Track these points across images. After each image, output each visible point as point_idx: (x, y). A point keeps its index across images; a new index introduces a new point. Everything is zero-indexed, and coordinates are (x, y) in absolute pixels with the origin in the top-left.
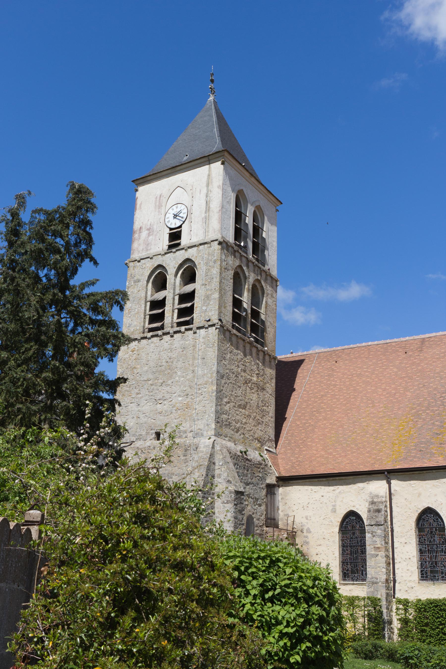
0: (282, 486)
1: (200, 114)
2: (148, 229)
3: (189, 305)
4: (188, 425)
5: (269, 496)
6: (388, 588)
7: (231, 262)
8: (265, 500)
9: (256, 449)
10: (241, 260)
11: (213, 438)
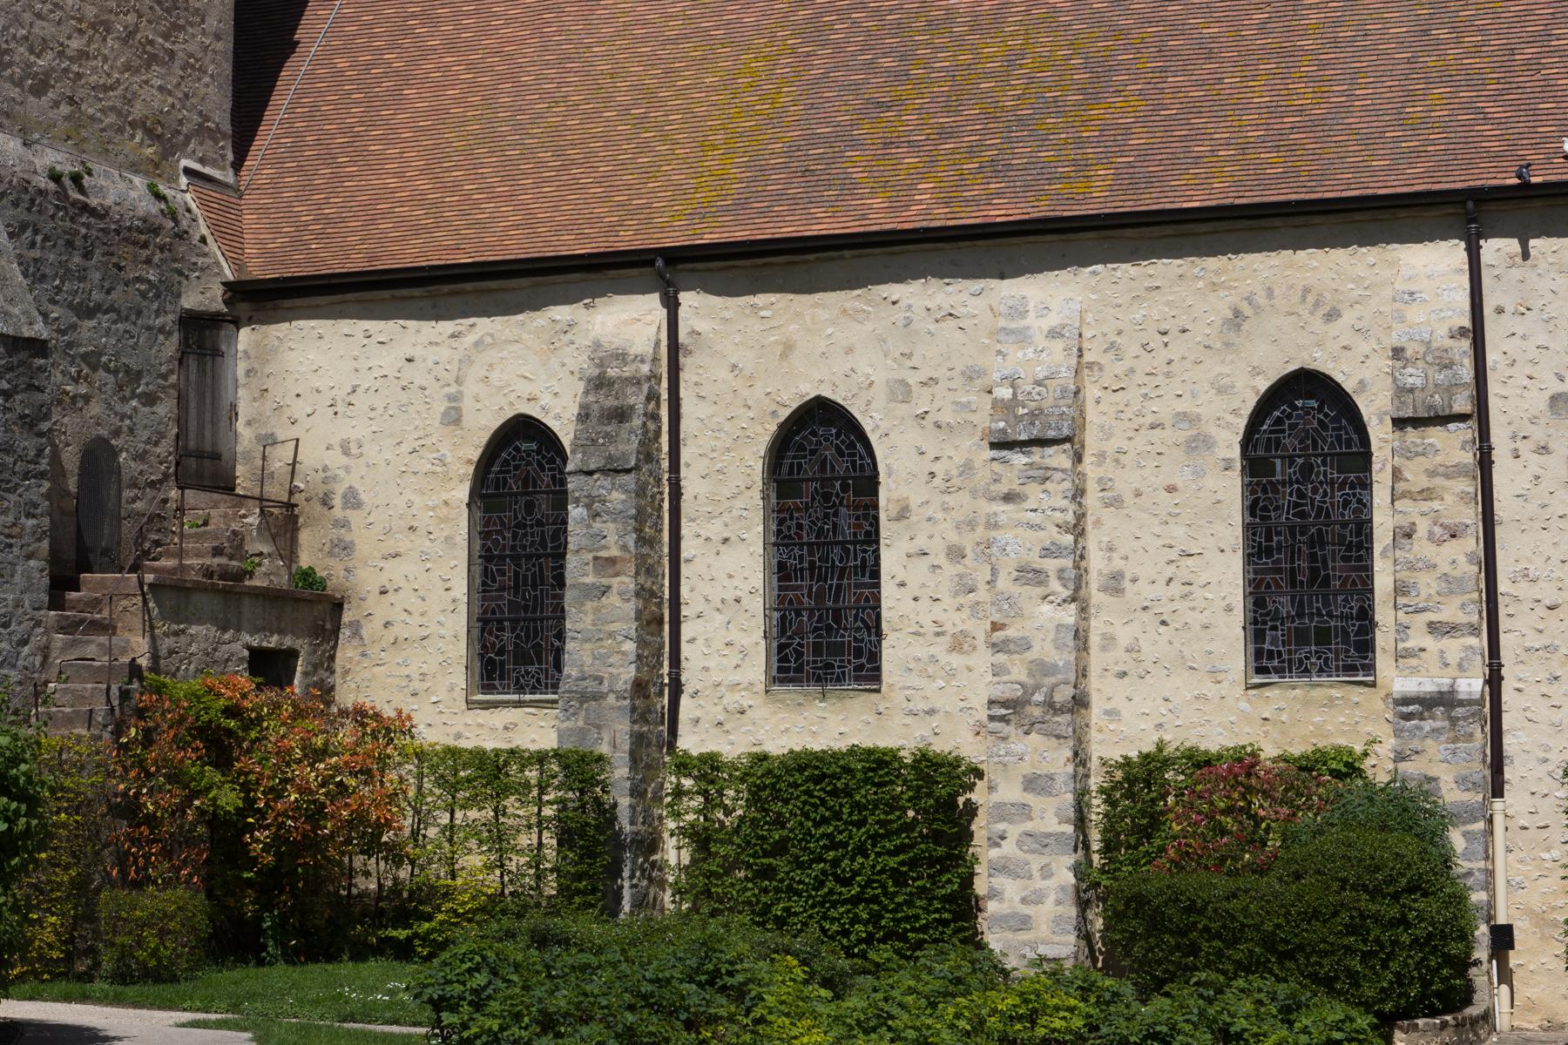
0: (250, 321)
5: (192, 363)
6: (640, 715)
8: (173, 378)
9: (135, 168)
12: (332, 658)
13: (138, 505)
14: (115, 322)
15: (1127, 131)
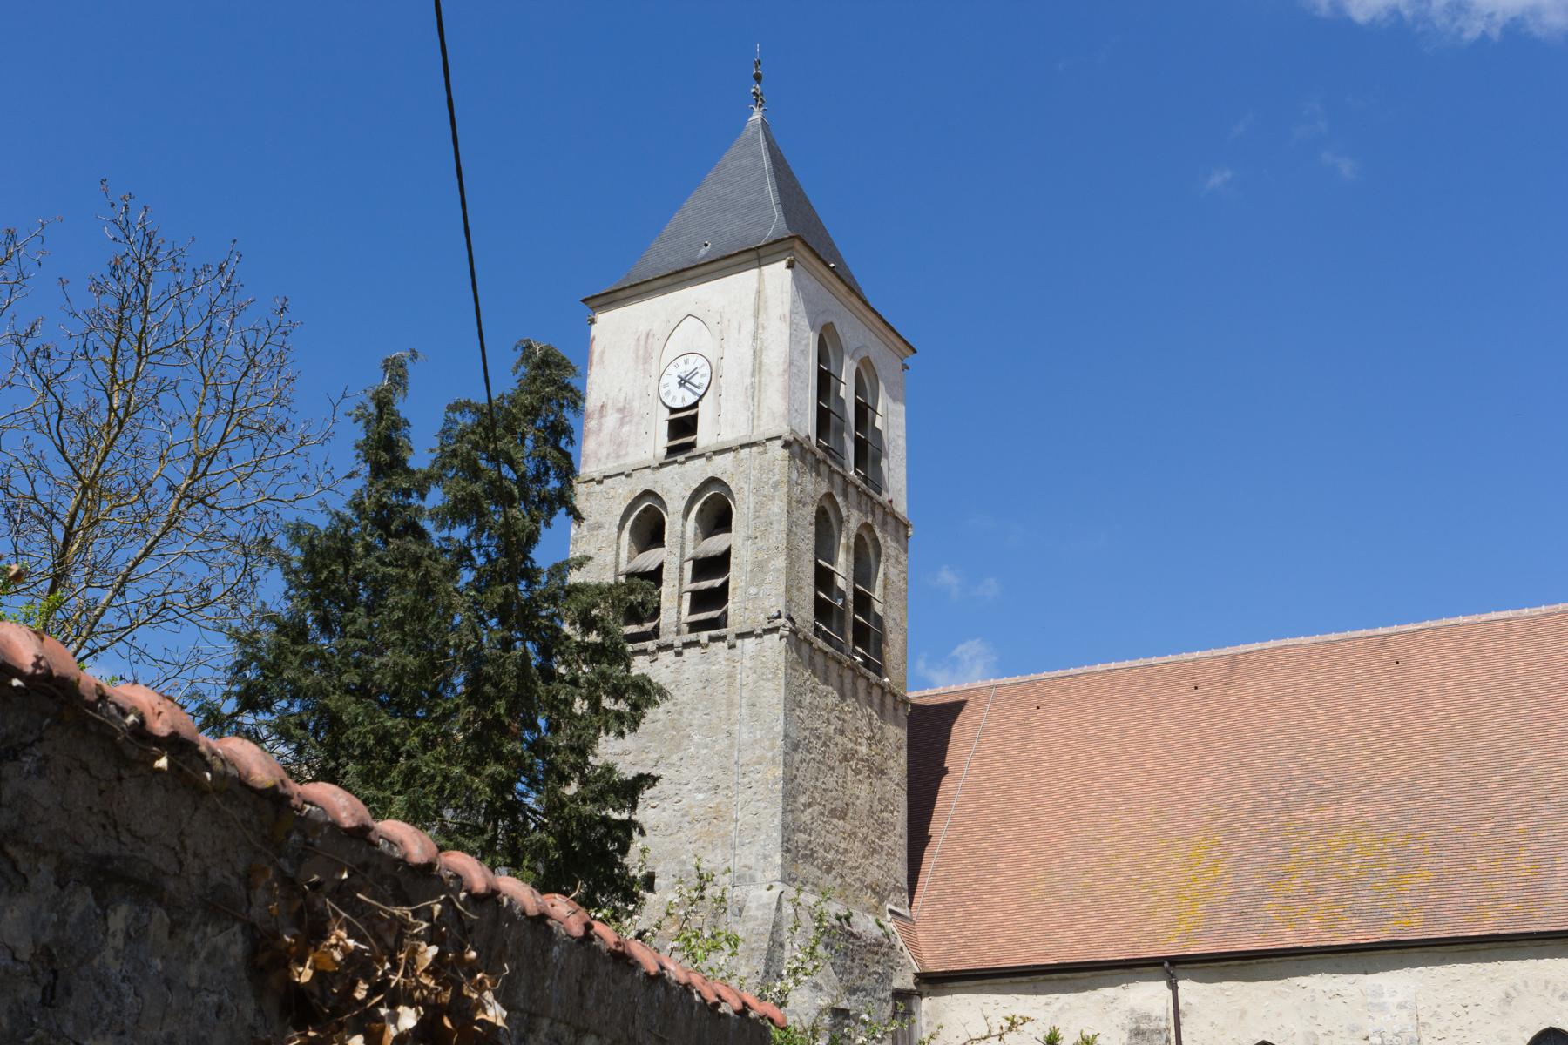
0: (928, 994)
1: (733, 150)
2: (620, 410)
3: (717, 582)
4: (720, 858)
7: (810, 487)
9: (868, 910)
10: (831, 481)
11: (778, 887)
15: (1426, 890)
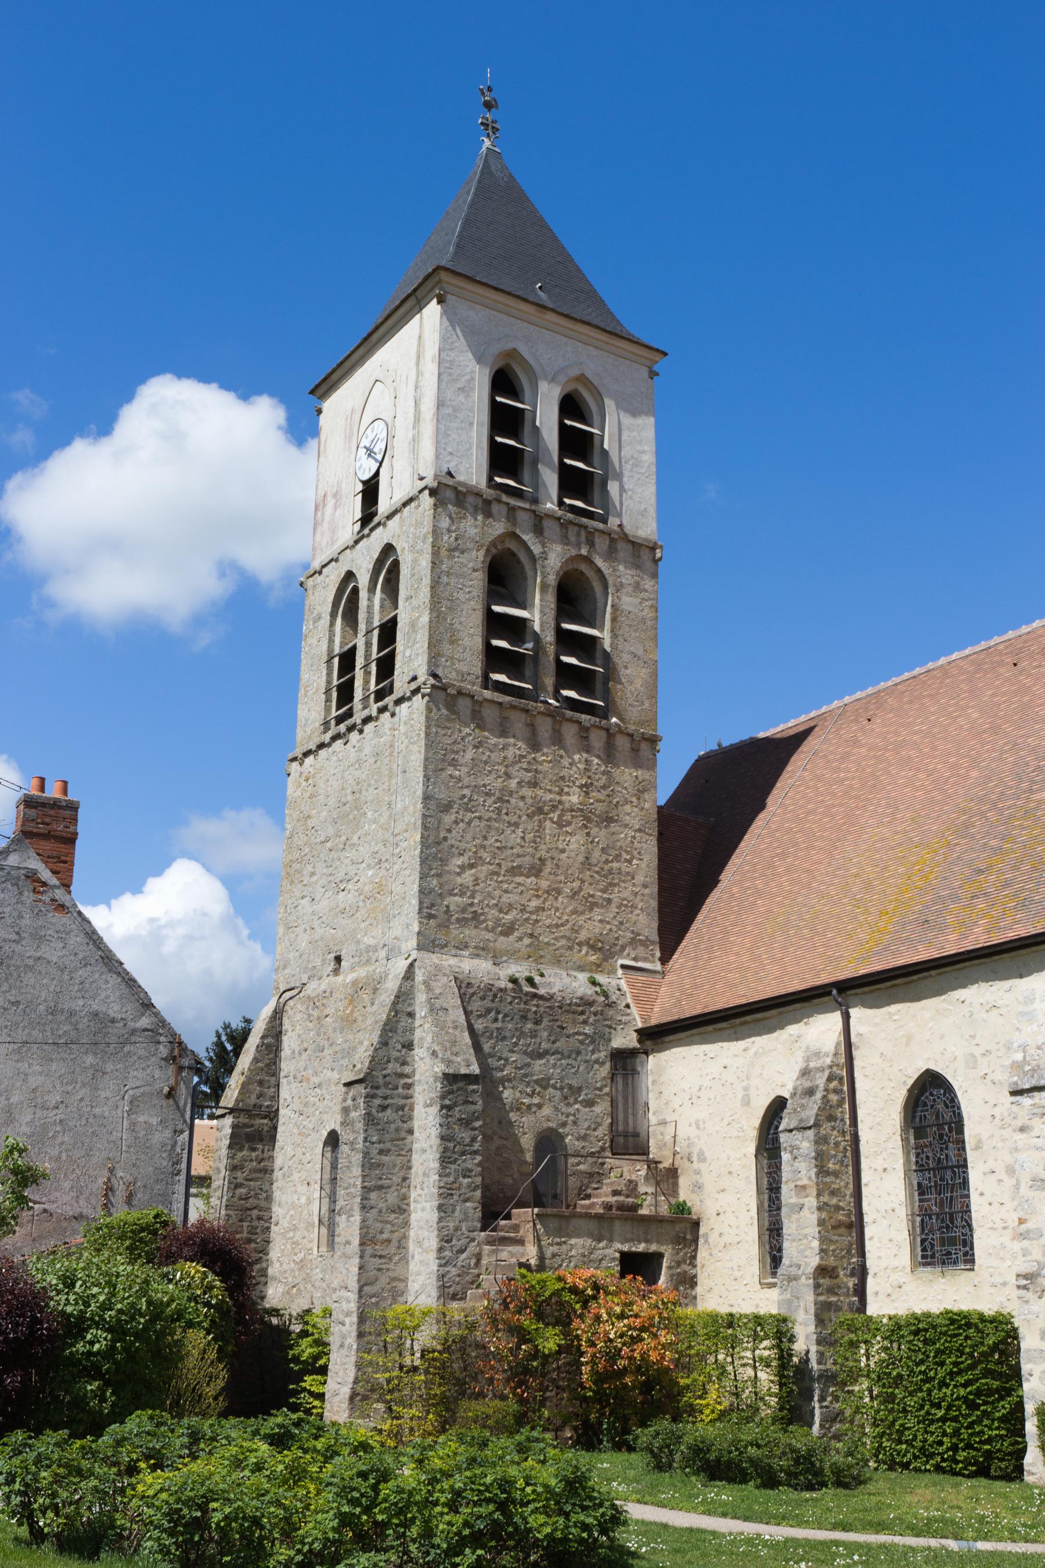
0: (653, 1051)
5: (620, 1080)
8: (607, 1090)
9: (581, 969)
12: (694, 1257)
13: (582, 1167)
14: (560, 1060)
